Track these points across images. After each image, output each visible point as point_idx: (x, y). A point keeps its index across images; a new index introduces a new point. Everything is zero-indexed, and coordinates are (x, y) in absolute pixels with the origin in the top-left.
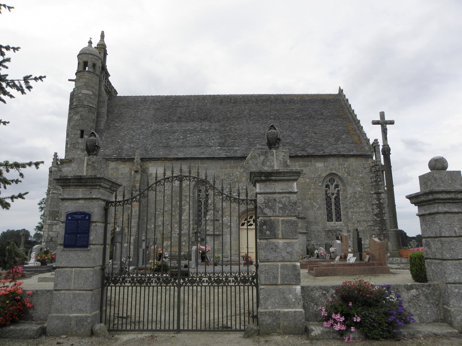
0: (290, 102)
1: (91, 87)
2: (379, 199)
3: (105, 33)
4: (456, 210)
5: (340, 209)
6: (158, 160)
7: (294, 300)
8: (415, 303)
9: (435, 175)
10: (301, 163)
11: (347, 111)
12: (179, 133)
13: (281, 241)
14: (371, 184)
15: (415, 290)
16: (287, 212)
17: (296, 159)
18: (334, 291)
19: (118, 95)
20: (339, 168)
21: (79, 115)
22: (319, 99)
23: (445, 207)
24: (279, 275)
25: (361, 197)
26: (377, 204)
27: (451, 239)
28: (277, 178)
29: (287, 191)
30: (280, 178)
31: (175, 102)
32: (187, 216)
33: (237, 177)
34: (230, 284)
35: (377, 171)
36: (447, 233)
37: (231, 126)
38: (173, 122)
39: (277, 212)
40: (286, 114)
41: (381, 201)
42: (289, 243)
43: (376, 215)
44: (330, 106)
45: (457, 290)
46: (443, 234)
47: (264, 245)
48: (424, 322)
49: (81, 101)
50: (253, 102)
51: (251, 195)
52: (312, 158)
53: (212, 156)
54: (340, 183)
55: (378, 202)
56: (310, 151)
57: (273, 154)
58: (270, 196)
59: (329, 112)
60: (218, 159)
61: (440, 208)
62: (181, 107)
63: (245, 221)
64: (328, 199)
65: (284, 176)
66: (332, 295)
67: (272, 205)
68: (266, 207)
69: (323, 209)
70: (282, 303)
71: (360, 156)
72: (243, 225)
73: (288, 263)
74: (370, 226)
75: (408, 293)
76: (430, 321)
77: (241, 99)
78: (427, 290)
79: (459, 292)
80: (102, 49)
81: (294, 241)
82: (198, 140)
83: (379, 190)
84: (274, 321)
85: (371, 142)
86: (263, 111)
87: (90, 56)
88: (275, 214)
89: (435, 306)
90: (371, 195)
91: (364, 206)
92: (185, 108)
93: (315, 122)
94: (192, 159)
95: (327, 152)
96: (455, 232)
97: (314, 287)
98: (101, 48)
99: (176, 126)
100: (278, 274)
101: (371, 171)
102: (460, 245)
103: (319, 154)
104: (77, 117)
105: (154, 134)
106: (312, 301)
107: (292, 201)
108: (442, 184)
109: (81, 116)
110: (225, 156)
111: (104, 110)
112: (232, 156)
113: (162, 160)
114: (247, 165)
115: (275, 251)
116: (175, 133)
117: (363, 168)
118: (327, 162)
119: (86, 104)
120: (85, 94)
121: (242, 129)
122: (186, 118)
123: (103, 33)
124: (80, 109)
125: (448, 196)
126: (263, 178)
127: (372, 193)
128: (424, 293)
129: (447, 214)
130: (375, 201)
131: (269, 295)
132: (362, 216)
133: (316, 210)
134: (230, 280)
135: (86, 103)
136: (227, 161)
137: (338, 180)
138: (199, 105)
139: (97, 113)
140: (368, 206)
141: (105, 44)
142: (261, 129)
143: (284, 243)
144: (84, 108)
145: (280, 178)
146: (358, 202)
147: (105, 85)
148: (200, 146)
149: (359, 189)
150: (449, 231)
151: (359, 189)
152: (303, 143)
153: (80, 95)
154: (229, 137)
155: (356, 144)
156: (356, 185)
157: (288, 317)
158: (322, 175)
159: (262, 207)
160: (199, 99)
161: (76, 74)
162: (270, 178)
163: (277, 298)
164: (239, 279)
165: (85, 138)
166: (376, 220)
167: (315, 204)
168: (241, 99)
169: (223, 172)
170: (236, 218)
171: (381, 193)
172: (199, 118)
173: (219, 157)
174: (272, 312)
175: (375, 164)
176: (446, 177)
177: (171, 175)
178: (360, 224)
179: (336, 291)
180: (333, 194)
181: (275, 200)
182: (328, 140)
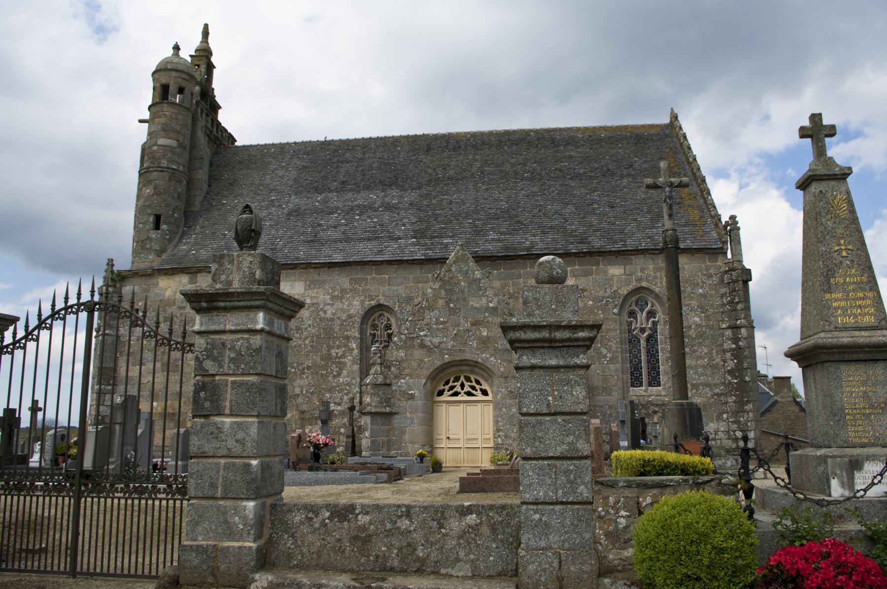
0: (568, 144)
1: (174, 132)
2: (736, 340)
3: (209, 27)
4: (553, 362)
5: (658, 360)
6: (293, 269)
7: (241, 526)
8: (470, 540)
9: (526, 293)
10: (577, 267)
11: (684, 159)
12: (339, 214)
13: (228, 420)
14: (721, 310)
15: (474, 515)
16: (242, 366)
17: (347, 268)
18: (327, 514)
19: (236, 144)
20: (656, 277)
21: (151, 187)
22: (629, 134)
23: (535, 357)
24: (221, 480)
25: (701, 335)
26: (733, 350)
27: (540, 418)
28: (228, 304)
29: (244, 327)
30: (232, 304)
31: (338, 152)
32: (348, 377)
33: (427, 300)
34: (159, 496)
35: (734, 282)
36: (532, 407)
37: (442, 197)
38: (330, 192)
39: (226, 367)
40: (556, 169)
41: (740, 343)
42: (241, 423)
43: (730, 372)
44: (649, 148)
45: (537, 516)
46: (525, 409)
47: (199, 427)
48: (479, 576)
49: (157, 159)
50: (491, 146)
51: (455, 334)
52: (601, 258)
53: (398, 258)
54: (657, 307)
55: (734, 346)
56: (597, 243)
57: (233, 260)
58: (216, 337)
59: (645, 161)
60: (411, 264)
61: (525, 358)
62: (348, 163)
63: (444, 385)
64: (633, 341)
65: (240, 301)
66: (324, 520)
67: (218, 353)
68: (208, 357)
69: (620, 361)
70: (220, 531)
71: (699, 250)
72: (441, 393)
73: (238, 461)
74: (717, 394)
75: (460, 521)
76: (492, 573)
77: (469, 140)
78: (497, 516)
79: (541, 519)
80: (204, 58)
81: (250, 420)
82: (375, 227)
83: (737, 320)
84: (203, 562)
85: (725, 219)
86: (510, 163)
87: (174, 74)
88: (221, 370)
89: (506, 545)
90: (721, 331)
91: (706, 354)
92: (355, 164)
93: (613, 183)
94: (359, 265)
95: (631, 244)
96: (548, 405)
97: (295, 505)
98: (202, 56)
99: (335, 200)
100: (218, 479)
101: (722, 280)
102: (555, 430)
103: (613, 249)
104: (148, 191)
105: (292, 218)
106: (286, 532)
107: (253, 347)
108: (537, 312)
109: (155, 189)
110: (423, 257)
111: (202, 175)
112: (436, 257)
113: (302, 268)
114: (447, 274)
115: (217, 438)
116: (332, 214)
117: (705, 275)
118: (631, 264)
119: (165, 165)
120: (163, 146)
121: (463, 202)
122: (356, 184)
123: (206, 27)
124: (155, 175)
125: (536, 335)
126: (204, 305)
127: (724, 326)
128: (490, 521)
129: (537, 370)
130: (729, 344)
131: (200, 516)
132: (702, 375)
133: (606, 362)
134: (160, 489)
135: (164, 163)
136: (427, 267)
137: (654, 301)
138: (383, 156)
139: (187, 181)
140: (714, 354)
141: (209, 48)
142: (501, 201)
143: (233, 423)
144: (161, 173)
145: (232, 304)
146: (694, 345)
147: (206, 126)
148: (377, 238)
149: (697, 319)
150: (537, 402)
151: (697, 319)
152: (584, 226)
153: (155, 148)
154: (436, 219)
155: (695, 226)
156: (691, 311)
157: (227, 557)
158: (619, 291)
159: (201, 358)
160: (385, 145)
161: (150, 108)
162: (215, 304)
163: (214, 522)
164: (174, 486)
165: (163, 230)
166: (730, 383)
167: (604, 351)
168: (469, 140)
169: (419, 290)
170: (424, 381)
171: (740, 327)
172: (380, 182)
173: (411, 258)
174: (201, 546)
175: (729, 267)
176: (548, 298)
177: (75, 301)
178: (697, 391)
179: (331, 514)
180: (643, 330)
181: (223, 344)
182: (636, 220)
